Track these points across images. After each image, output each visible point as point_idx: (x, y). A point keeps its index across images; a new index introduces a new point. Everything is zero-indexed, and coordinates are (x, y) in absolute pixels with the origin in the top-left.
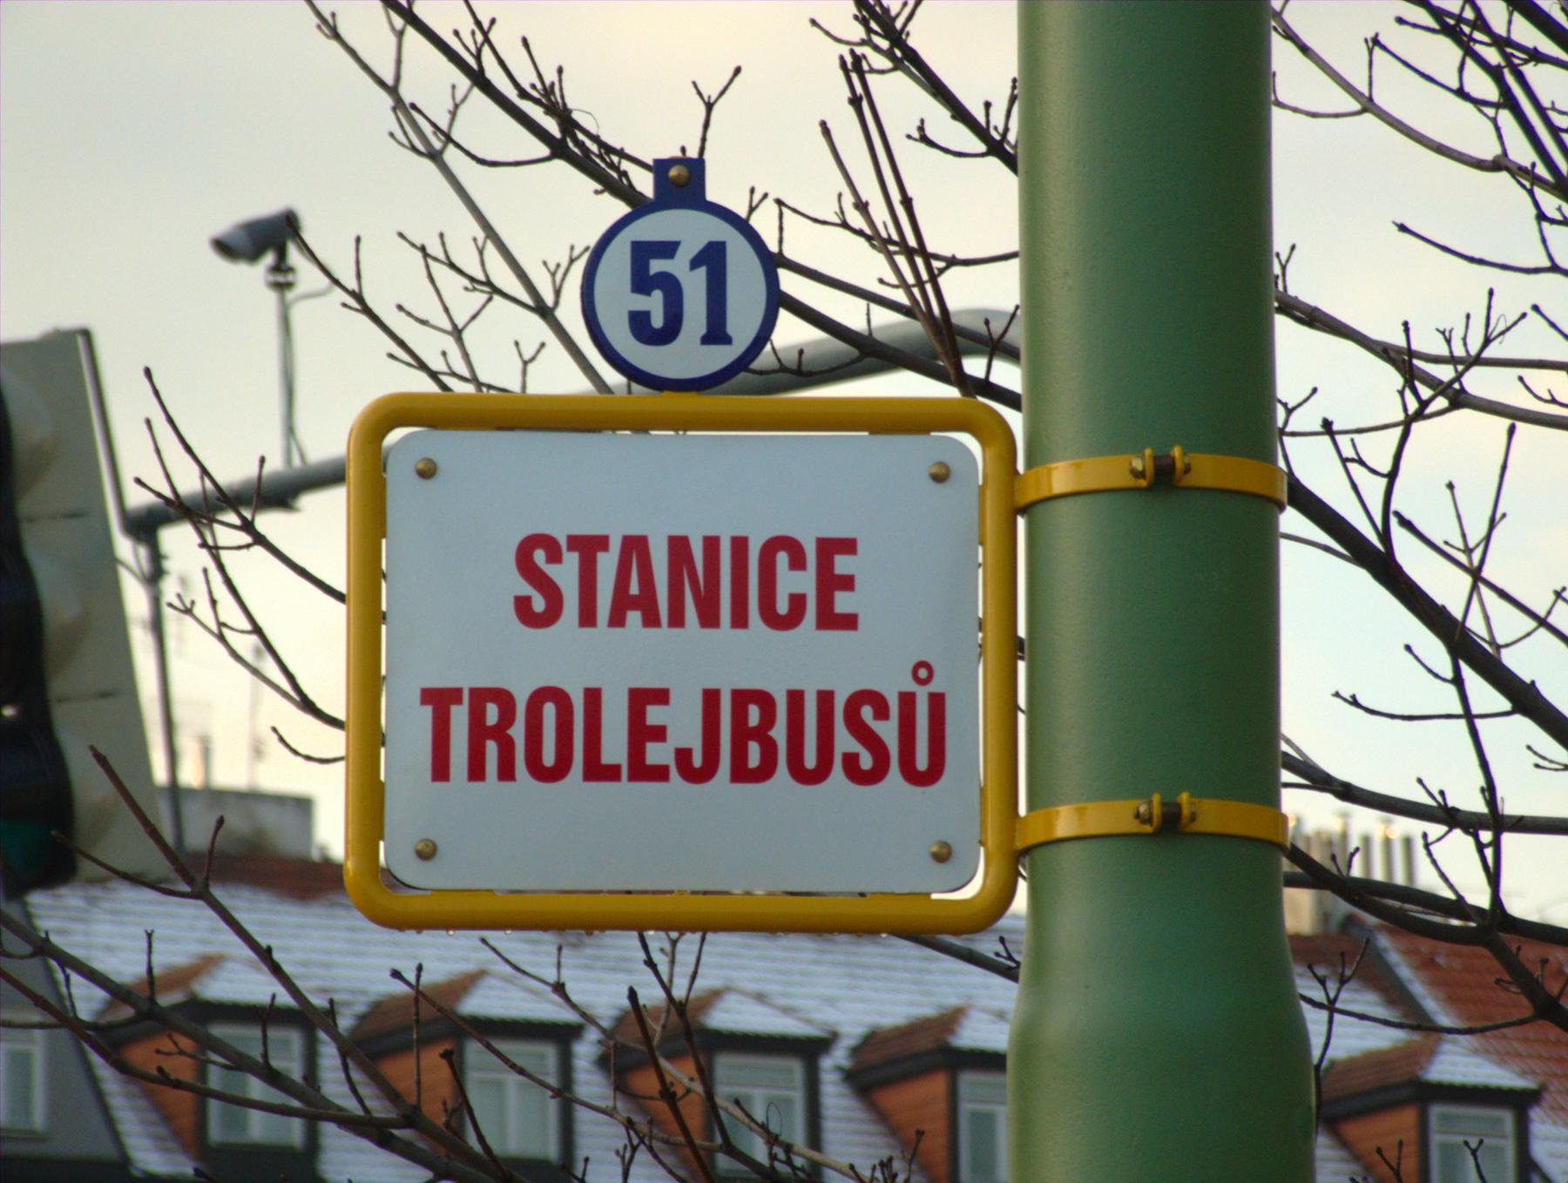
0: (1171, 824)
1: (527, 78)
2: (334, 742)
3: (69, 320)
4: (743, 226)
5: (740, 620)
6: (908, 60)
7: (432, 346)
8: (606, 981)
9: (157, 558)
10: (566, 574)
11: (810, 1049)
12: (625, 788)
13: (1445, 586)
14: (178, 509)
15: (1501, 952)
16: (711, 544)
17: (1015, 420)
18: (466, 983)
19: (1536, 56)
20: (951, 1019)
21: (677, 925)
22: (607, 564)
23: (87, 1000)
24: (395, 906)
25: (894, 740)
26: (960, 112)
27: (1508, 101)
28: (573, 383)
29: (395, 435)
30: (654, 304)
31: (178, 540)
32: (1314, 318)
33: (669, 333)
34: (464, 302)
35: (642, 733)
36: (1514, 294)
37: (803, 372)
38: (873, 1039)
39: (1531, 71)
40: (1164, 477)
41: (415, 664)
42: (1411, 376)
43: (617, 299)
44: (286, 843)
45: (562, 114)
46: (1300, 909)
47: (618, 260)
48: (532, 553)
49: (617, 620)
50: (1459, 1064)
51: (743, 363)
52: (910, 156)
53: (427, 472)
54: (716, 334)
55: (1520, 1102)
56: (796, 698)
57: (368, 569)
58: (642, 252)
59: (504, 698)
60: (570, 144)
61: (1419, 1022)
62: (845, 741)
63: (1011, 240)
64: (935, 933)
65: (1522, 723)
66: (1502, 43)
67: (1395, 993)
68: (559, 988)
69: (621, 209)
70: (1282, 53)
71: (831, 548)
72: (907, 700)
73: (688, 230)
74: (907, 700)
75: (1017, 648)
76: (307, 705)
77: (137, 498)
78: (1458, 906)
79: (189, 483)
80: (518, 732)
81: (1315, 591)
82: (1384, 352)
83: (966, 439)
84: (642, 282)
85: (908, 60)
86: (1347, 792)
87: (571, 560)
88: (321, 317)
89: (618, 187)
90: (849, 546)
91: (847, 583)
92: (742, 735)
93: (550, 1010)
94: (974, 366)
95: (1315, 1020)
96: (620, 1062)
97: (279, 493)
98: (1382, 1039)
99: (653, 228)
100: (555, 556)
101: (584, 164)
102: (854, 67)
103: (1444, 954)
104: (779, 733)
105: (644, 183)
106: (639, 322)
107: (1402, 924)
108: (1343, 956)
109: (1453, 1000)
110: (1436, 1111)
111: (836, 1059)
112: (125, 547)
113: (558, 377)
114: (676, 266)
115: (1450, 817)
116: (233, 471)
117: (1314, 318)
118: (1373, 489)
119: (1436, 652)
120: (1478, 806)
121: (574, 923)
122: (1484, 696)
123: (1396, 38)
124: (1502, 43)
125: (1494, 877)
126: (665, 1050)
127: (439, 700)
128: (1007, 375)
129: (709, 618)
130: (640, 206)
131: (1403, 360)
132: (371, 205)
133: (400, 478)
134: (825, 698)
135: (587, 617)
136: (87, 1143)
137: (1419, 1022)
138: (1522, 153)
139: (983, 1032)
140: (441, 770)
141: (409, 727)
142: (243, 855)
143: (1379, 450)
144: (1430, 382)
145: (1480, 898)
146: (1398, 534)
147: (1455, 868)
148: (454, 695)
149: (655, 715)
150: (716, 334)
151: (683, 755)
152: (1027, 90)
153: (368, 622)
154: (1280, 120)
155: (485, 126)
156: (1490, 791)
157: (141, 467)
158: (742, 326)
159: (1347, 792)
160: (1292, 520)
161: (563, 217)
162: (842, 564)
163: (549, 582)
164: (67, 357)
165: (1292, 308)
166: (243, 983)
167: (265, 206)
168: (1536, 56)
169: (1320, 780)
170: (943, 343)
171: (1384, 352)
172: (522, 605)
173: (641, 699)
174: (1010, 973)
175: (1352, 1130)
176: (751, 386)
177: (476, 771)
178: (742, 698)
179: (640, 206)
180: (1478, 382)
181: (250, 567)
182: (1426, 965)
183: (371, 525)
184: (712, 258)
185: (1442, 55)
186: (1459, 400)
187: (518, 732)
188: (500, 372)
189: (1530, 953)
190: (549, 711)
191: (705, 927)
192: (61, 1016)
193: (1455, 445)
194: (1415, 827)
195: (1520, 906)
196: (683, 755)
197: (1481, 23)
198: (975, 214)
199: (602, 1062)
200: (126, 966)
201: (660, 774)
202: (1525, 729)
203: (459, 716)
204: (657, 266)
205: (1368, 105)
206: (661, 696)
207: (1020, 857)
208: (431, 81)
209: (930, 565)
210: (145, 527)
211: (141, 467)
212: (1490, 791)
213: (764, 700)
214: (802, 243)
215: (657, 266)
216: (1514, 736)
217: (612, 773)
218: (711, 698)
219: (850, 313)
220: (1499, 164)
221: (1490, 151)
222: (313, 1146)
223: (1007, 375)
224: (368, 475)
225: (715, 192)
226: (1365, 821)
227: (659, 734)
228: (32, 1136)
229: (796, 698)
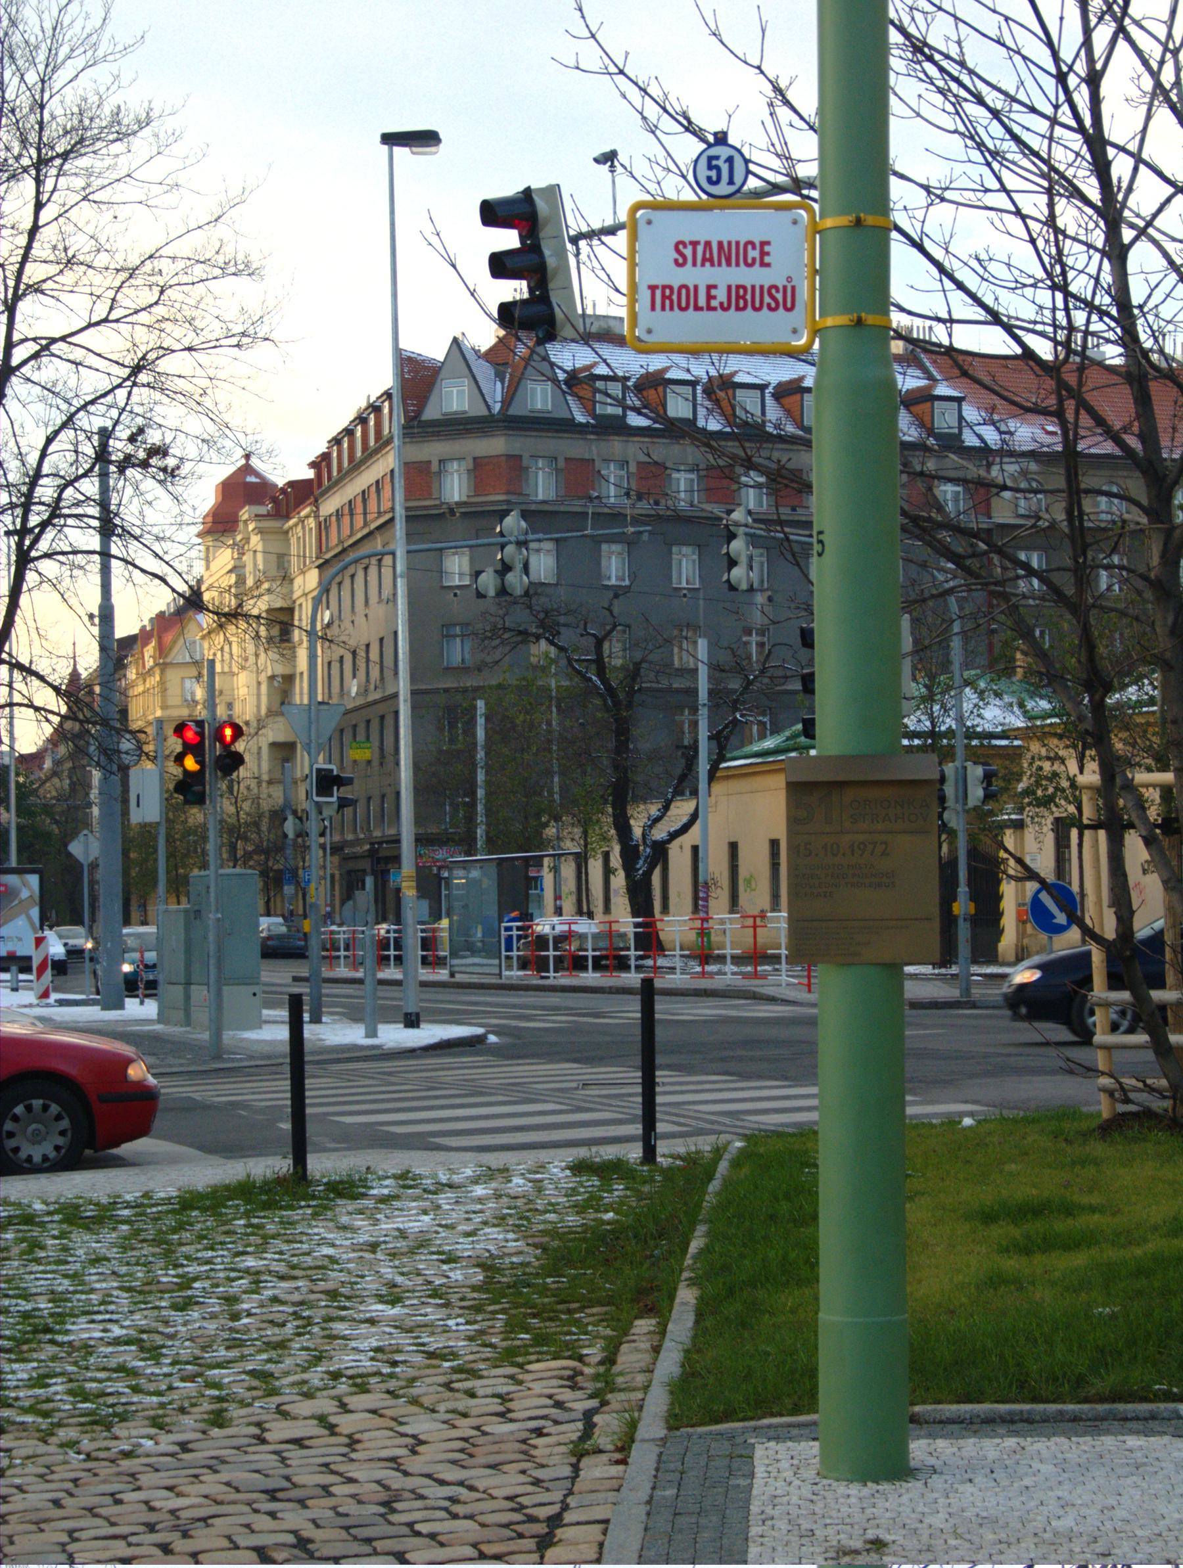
0: (859, 322)
1: (678, 109)
2: (624, 300)
3: (554, 182)
4: (739, 151)
5: (737, 264)
6: (787, 103)
7: (652, 187)
8: (701, 369)
9: (578, 249)
10: (688, 252)
11: (762, 388)
12: (705, 313)
13: (938, 254)
14: (581, 236)
15: (952, 358)
16: (729, 243)
17: (816, 206)
18: (666, 369)
19: (966, 100)
20: (801, 379)
21: (721, 352)
22: (700, 249)
23: (561, 376)
24: (644, 349)
25: (780, 299)
26: (802, 118)
27: (957, 113)
28: (692, 197)
29: (639, 214)
30: (713, 174)
31: (583, 244)
32: (902, 177)
33: (718, 182)
34: (661, 174)
35: (710, 297)
36: (959, 168)
37: (757, 194)
38: (780, 384)
39: (964, 104)
40: (858, 222)
41: (645, 279)
42: (929, 193)
43: (703, 172)
44: (617, 331)
45: (690, 122)
46: (897, 347)
47: (703, 162)
48: (679, 246)
49: (703, 265)
50: (942, 390)
51: (738, 191)
52: (787, 130)
53: (649, 222)
54: (731, 182)
55: (959, 400)
56: (753, 287)
57: (632, 251)
58: (710, 159)
59: (671, 288)
60: (690, 127)
61: (930, 377)
62: (767, 299)
63: (816, 155)
64: (794, 354)
65: (959, 292)
66: (955, 96)
67: (925, 371)
68: (688, 371)
69: (704, 146)
70: (893, 100)
71: (763, 244)
72: (785, 288)
73: (722, 152)
74: (785, 288)
75: (816, 272)
76: (617, 290)
77: (572, 233)
78: (940, 345)
79: (585, 229)
80: (675, 297)
81: (900, 253)
82: (921, 186)
83: (802, 212)
84: (710, 167)
85: (787, 103)
86: (910, 313)
87: (690, 248)
88: (622, 179)
89: (703, 140)
90: (768, 243)
91: (768, 254)
92: (738, 297)
93: (688, 377)
94: (805, 192)
95: (899, 378)
96: (709, 392)
97: (611, 231)
98: (922, 383)
99: (714, 151)
100: (685, 246)
101: (694, 133)
102: (771, 105)
103: (939, 359)
104: (749, 297)
105: (711, 139)
106: (709, 179)
107: (926, 351)
108: (910, 360)
109: (941, 372)
110: (936, 403)
111: (770, 389)
112: (569, 246)
113: (688, 195)
114: (720, 162)
115: (939, 320)
116: (596, 226)
117: (902, 177)
118: (918, 226)
119: (934, 271)
120: (946, 316)
121: (694, 352)
122: (948, 285)
123: (925, 94)
124: (955, 96)
125: (950, 336)
126: (721, 389)
127: (653, 288)
128: (814, 194)
129: (729, 264)
130: (710, 145)
131: (927, 188)
132: (636, 148)
133: (642, 226)
134: (762, 287)
135: (694, 264)
136: (564, 414)
137: (930, 377)
138: (962, 129)
139: (808, 383)
140: (653, 308)
141: (644, 295)
142: (602, 334)
143: (920, 214)
144: (935, 194)
145: (946, 342)
146: (925, 239)
147: (940, 334)
148: (656, 287)
149: (713, 292)
150: (731, 182)
151: (721, 304)
152: (821, 112)
153: (632, 266)
154: (892, 118)
155: (667, 124)
156: (949, 312)
157: (575, 224)
158: (738, 179)
159: (910, 313)
160: (894, 235)
161: (688, 149)
162: (767, 248)
163: (682, 253)
164: (553, 192)
165: (896, 174)
166: (602, 370)
167: (607, 149)
168: (966, 100)
169: (902, 309)
170: (797, 185)
171: (921, 186)
172: (676, 261)
173: (710, 287)
174: (813, 365)
175: (912, 409)
176: (738, 198)
177: (663, 308)
178: (738, 287)
179: (710, 145)
180: (948, 195)
181: (600, 250)
182: (934, 362)
183: (633, 238)
184: (730, 160)
185: (938, 99)
186: (943, 200)
187: (675, 297)
188: (671, 195)
189: (960, 358)
190: (684, 291)
191: (728, 353)
192: (555, 381)
193: (942, 211)
194: (928, 323)
195: (956, 345)
196: (721, 304)
197: (950, 90)
198: (806, 150)
199: (704, 391)
200: (568, 366)
201: (714, 309)
202: (960, 294)
203: (658, 293)
204: (714, 163)
205: (918, 115)
206: (715, 287)
207: (816, 332)
208: (652, 111)
209: (793, 248)
210: (575, 240)
211: (575, 224)
212: (949, 312)
213: (745, 288)
214: (756, 156)
215: (714, 163)
216: (957, 297)
217: (701, 309)
218: (729, 287)
219: (771, 177)
220: (955, 131)
221: (952, 128)
222: (625, 416)
223: (814, 194)
224: (633, 226)
225: (731, 141)
226: (918, 322)
227: (714, 297)
228: (465, 412)
229: (753, 287)
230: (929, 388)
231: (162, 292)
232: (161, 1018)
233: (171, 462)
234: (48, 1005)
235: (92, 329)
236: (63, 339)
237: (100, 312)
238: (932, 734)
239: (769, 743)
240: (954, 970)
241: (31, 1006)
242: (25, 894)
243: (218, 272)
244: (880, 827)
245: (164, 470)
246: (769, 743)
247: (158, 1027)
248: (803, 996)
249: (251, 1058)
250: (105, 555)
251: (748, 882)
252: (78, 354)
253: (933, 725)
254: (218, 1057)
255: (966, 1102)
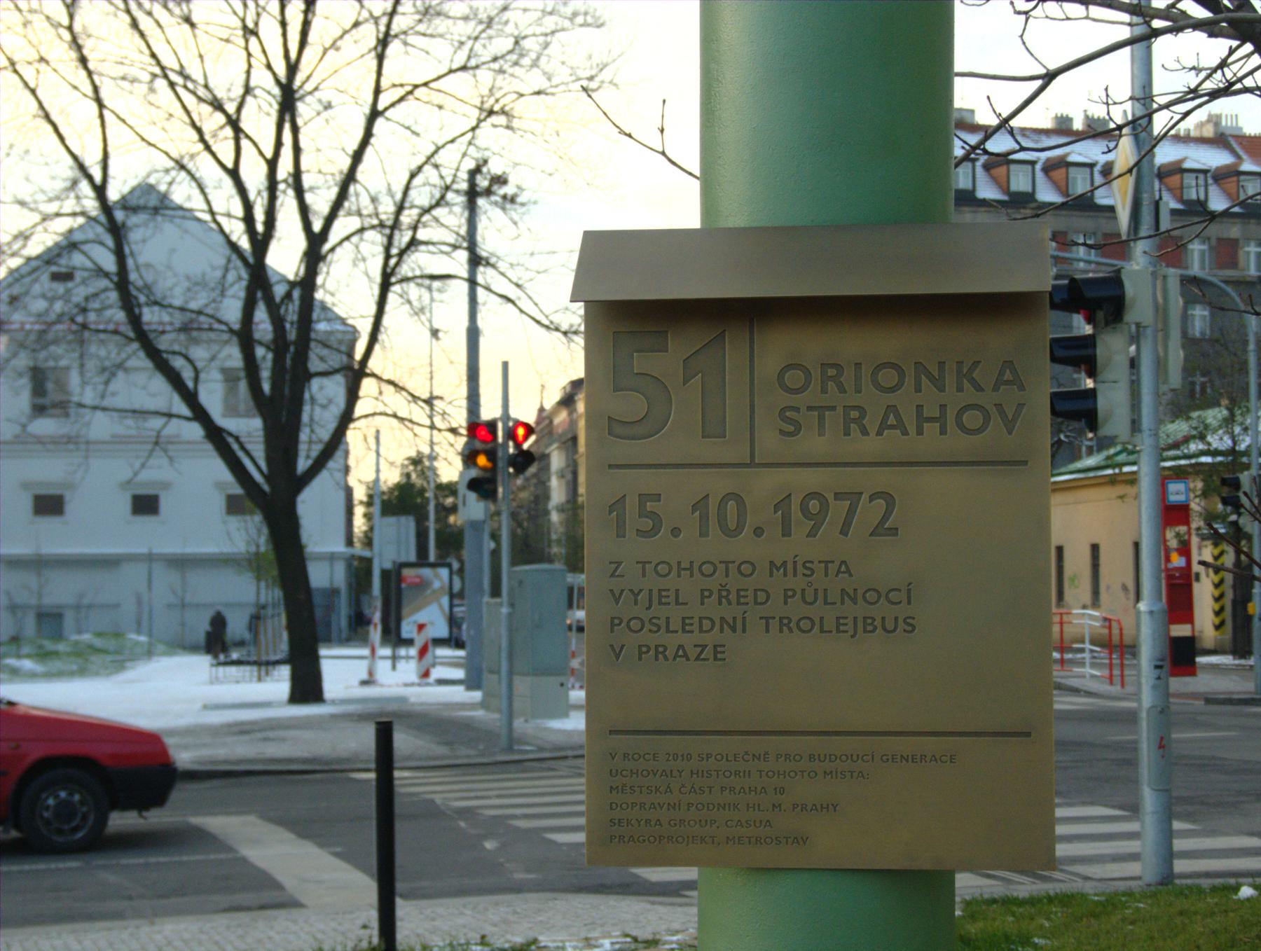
61: (1238, 157)
137: (1238, 157)
230: (1236, 165)
231: (517, 43)
232: (483, 705)
233: (509, 190)
234: (428, 684)
235: (452, 75)
236: (426, 84)
237: (460, 60)
238: (1232, 451)
239: (1091, 461)
240: (1251, 662)
241: (412, 685)
242: (437, 585)
243: (567, 24)
244: (871, 446)
245: (504, 197)
246: (1091, 461)
247: (480, 713)
248: (1104, 688)
249: (541, 749)
250: (472, 282)
251: (1072, 580)
252: (438, 98)
253: (1235, 443)
254: (510, 749)
255: (1252, 834)
